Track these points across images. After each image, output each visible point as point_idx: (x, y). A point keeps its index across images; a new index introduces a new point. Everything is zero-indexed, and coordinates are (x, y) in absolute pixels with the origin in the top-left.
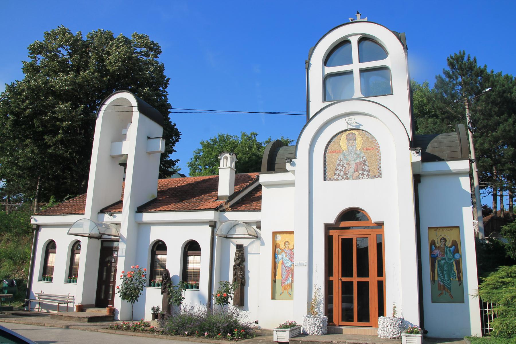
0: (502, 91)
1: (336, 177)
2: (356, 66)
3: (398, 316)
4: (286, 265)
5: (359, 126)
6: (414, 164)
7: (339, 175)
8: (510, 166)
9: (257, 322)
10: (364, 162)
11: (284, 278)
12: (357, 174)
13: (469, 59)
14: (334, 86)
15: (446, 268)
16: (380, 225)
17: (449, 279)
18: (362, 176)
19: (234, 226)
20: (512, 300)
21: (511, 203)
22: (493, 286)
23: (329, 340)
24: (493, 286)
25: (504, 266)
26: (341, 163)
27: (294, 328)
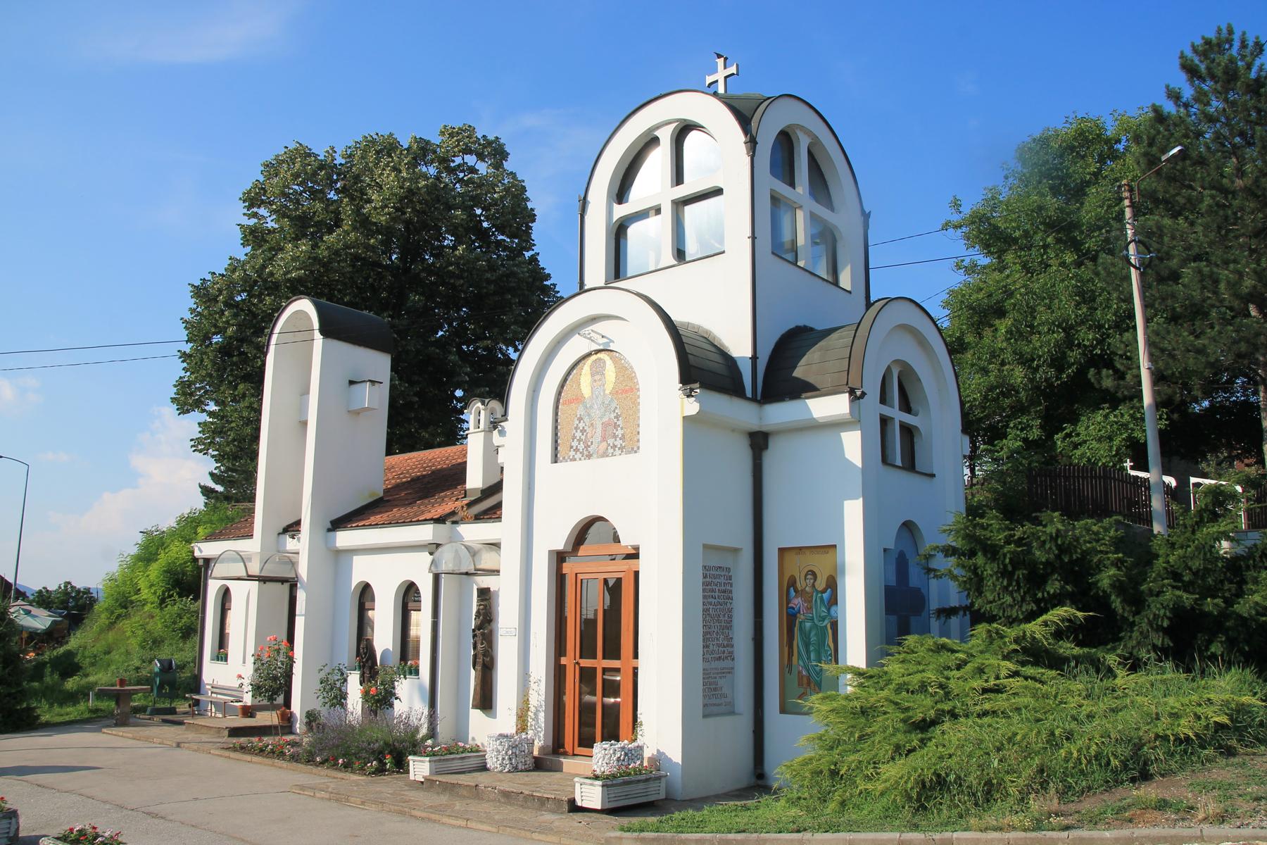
7: (577, 450)
15: (813, 639)
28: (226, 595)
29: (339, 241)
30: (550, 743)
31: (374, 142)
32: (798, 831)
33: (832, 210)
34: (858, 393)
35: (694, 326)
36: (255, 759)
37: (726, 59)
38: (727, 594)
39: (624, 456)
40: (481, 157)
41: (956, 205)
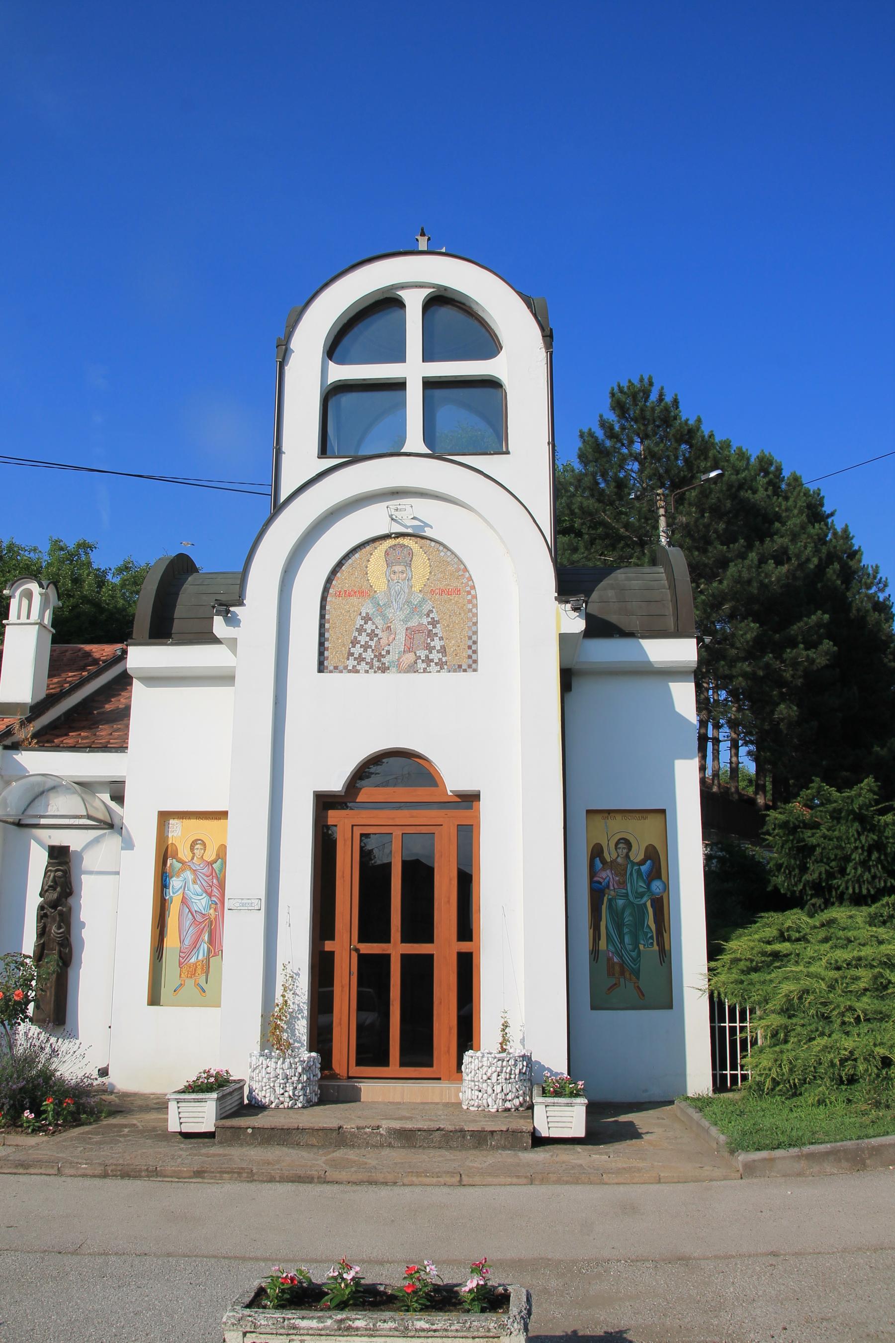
0: (736, 484)
1: (351, 663)
2: (414, 369)
3: (516, 1049)
4: (195, 908)
5: (422, 528)
6: (565, 639)
7: (360, 659)
8: (746, 667)
9: (104, 1072)
10: (430, 627)
11: (187, 942)
12: (410, 657)
13: (661, 399)
14: (353, 421)
15: (627, 918)
16: (470, 799)
17: (636, 946)
18: (424, 665)
19: (42, 793)
20: (800, 998)
21: (734, 759)
22: (748, 963)
23: (334, 1124)
24: (748, 963)
25: (772, 914)
26: (369, 627)
27: (227, 1090)
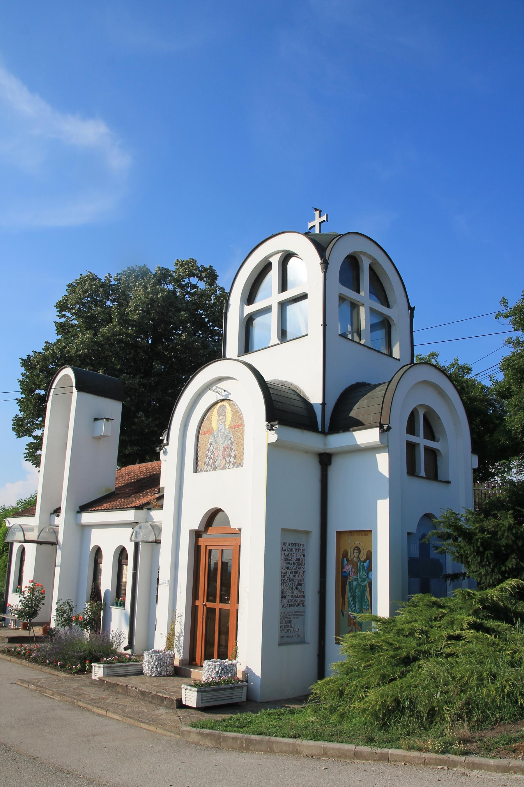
7: (208, 465)
15: (358, 594)
28: (22, 552)
29: (109, 331)
30: (187, 657)
31: (134, 271)
32: (295, 737)
33: (389, 307)
34: (385, 427)
35: (288, 383)
36: (13, 659)
37: (320, 212)
38: (301, 562)
39: (235, 469)
40: (200, 278)
41: (505, 302)
